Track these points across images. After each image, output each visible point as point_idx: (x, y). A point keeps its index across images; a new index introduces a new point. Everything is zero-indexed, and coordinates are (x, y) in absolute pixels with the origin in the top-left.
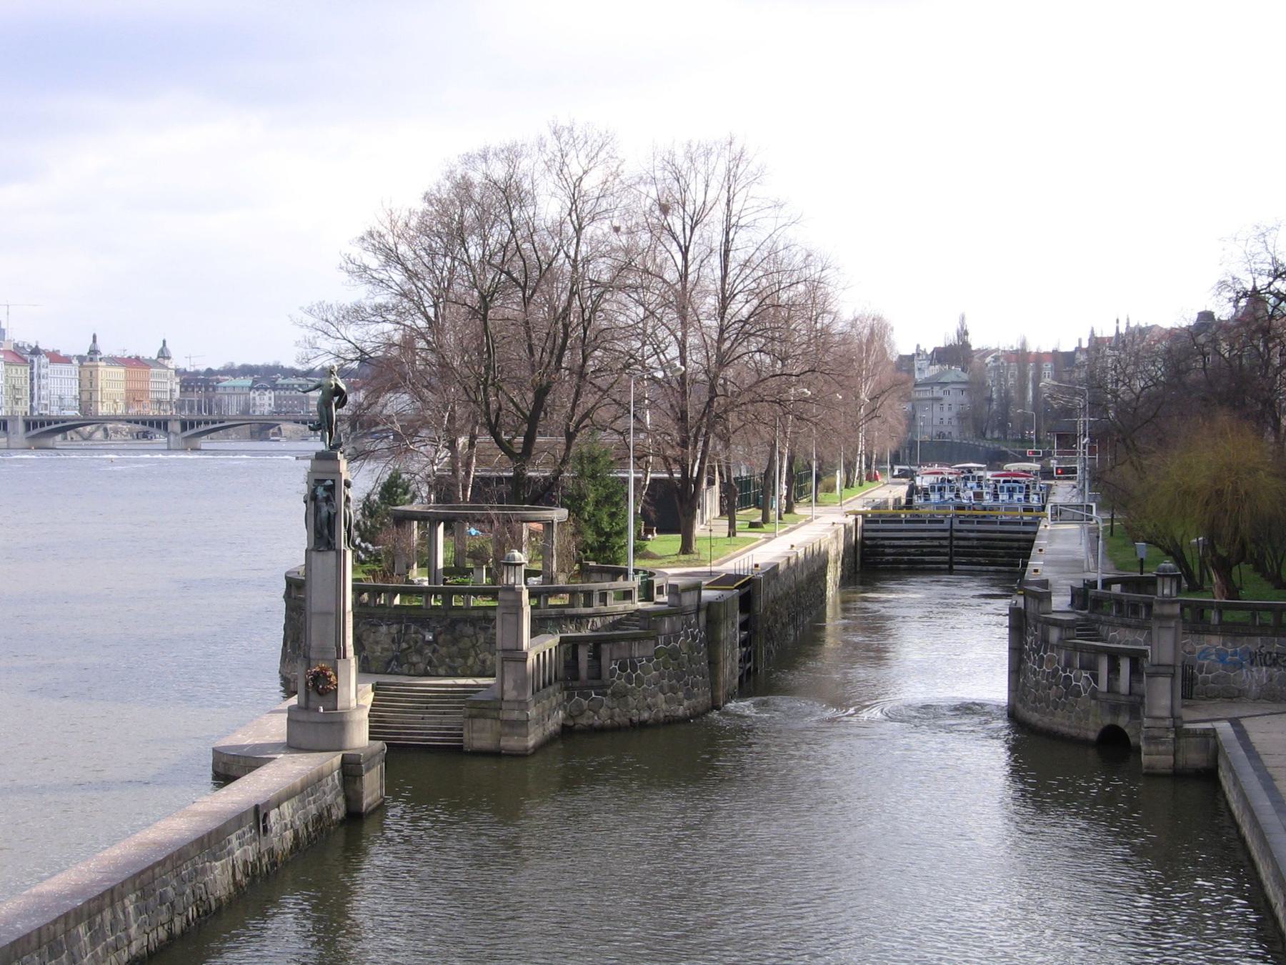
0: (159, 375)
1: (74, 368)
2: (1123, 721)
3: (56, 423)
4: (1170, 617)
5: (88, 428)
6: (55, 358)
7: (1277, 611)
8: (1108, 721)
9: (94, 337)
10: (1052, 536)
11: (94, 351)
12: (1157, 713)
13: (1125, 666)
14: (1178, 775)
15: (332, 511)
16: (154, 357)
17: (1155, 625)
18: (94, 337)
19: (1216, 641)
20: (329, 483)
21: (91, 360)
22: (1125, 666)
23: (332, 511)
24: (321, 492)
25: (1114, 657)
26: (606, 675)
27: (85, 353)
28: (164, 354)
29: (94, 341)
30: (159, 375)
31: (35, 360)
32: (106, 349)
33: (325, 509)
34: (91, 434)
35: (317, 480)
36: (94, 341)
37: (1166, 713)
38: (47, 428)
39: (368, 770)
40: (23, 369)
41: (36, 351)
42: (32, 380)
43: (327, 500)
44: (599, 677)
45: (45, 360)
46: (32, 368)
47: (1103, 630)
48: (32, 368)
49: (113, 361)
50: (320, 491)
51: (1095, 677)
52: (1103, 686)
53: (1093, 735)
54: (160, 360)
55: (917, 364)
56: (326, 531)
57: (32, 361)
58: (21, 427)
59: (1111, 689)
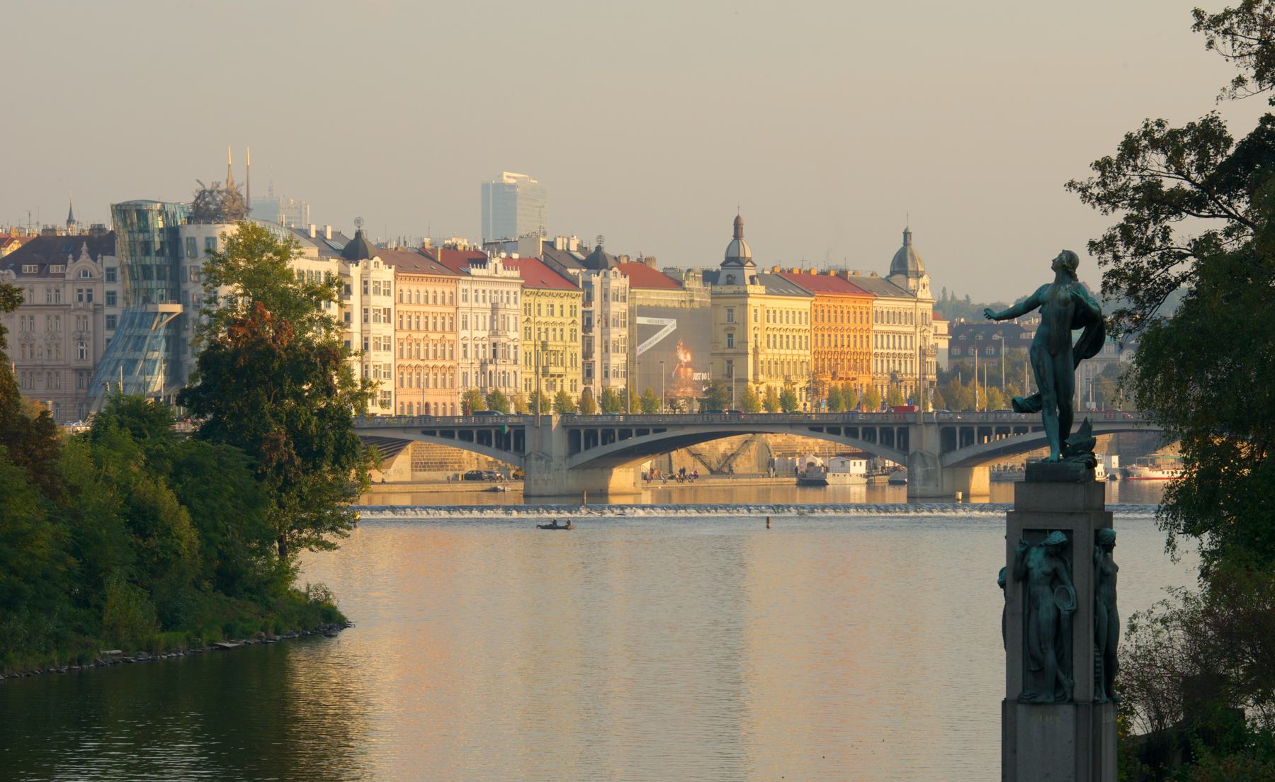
0: (896, 317)
3: (642, 432)
5: (723, 445)
6: (642, 274)
9: (737, 224)
10: (771, 315)
11: (734, 261)
15: (1066, 607)
16: (884, 272)
18: (737, 224)
20: (1058, 537)
21: (731, 281)
23: (1066, 607)
24: (1037, 561)
27: (715, 264)
28: (901, 264)
29: (737, 235)
30: (896, 317)
31: (596, 280)
33: (1047, 602)
34: (729, 458)
35: (1027, 531)
36: (737, 235)
38: (619, 445)
40: (567, 302)
41: (596, 261)
42: (587, 326)
43: (1054, 579)
45: (619, 282)
46: (588, 300)
48: (588, 300)
54: (898, 279)
56: (1051, 657)
57: (588, 285)
58: (558, 445)
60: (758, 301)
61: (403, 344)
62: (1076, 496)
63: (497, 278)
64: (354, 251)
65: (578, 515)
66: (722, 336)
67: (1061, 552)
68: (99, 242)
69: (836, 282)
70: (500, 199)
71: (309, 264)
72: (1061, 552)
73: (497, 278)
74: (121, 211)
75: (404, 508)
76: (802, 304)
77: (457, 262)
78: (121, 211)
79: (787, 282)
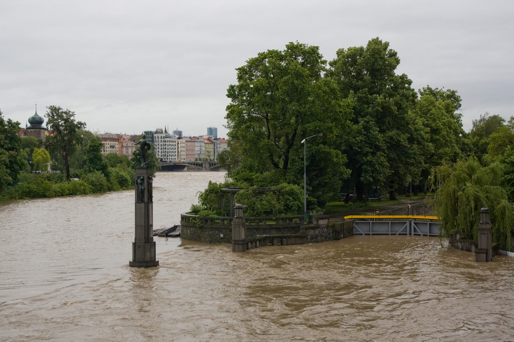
15: (143, 188)
20: (142, 177)
43: (141, 184)
67: (143, 180)
72: (143, 180)
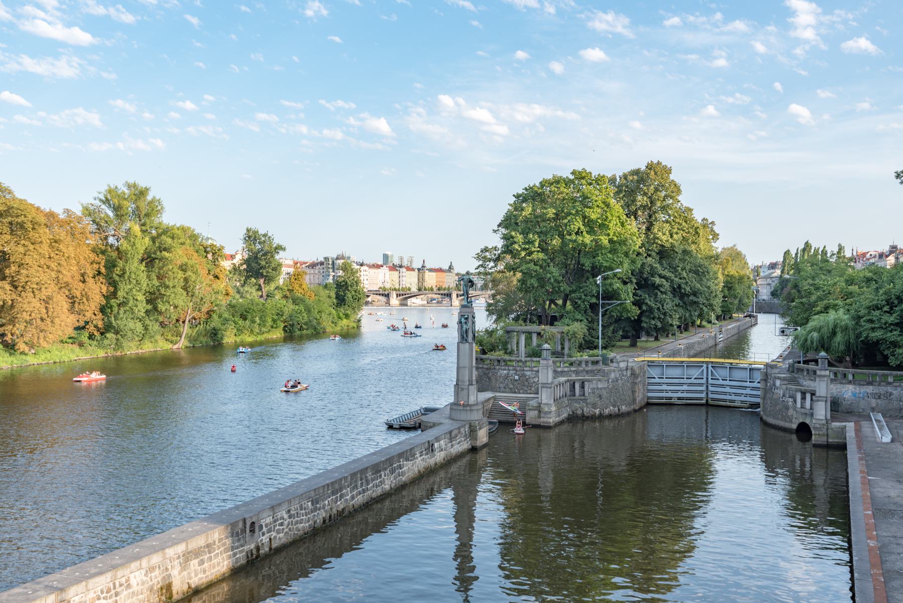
1: (416, 273)
2: (808, 421)
4: (824, 376)
7: (901, 376)
8: (801, 421)
11: (423, 267)
12: (818, 417)
13: (808, 396)
14: (828, 447)
17: (818, 379)
19: (851, 387)
22: (808, 396)
25: (804, 394)
26: (586, 394)
28: (451, 268)
32: (428, 266)
33: (465, 327)
37: (823, 418)
39: (480, 429)
44: (584, 395)
47: (801, 381)
49: (431, 270)
50: (463, 320)
51: (795, 401)
52: (799, 405)
53: (794, 426)
55: (761, 270)
59: (802, 407)
60: (427, 273)
61: (370, 280)
62: (469, 310)
63: (385, 269)
64: (362, 265)
65: (328, 105)
66: (421, 280)
67: (467, 319)
68: (322, 263)
69: (440, 270)
70: (386, 257)
71: (355, 267)
72: (467, 319)
73: (385, 269)
74: (325, 258)
75: (44, 20)
76: (434, 274)
77: (379, 267)
78: (325, 258)
79: (431, 270)
